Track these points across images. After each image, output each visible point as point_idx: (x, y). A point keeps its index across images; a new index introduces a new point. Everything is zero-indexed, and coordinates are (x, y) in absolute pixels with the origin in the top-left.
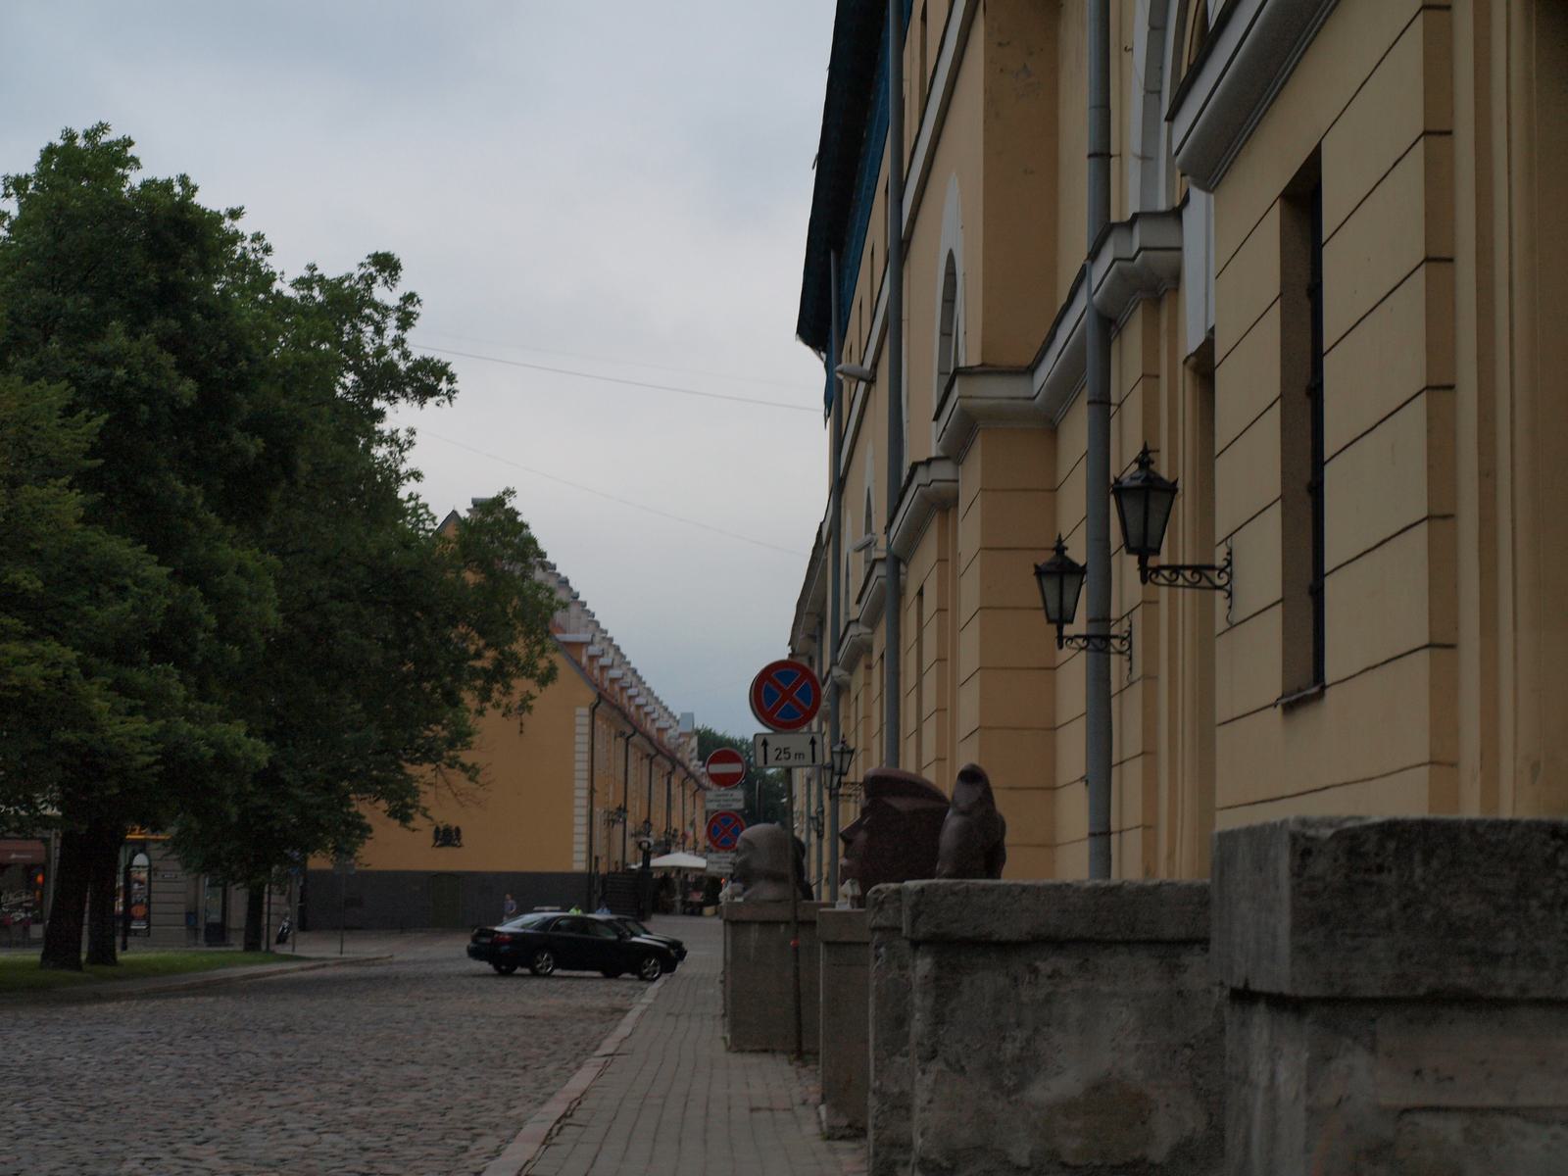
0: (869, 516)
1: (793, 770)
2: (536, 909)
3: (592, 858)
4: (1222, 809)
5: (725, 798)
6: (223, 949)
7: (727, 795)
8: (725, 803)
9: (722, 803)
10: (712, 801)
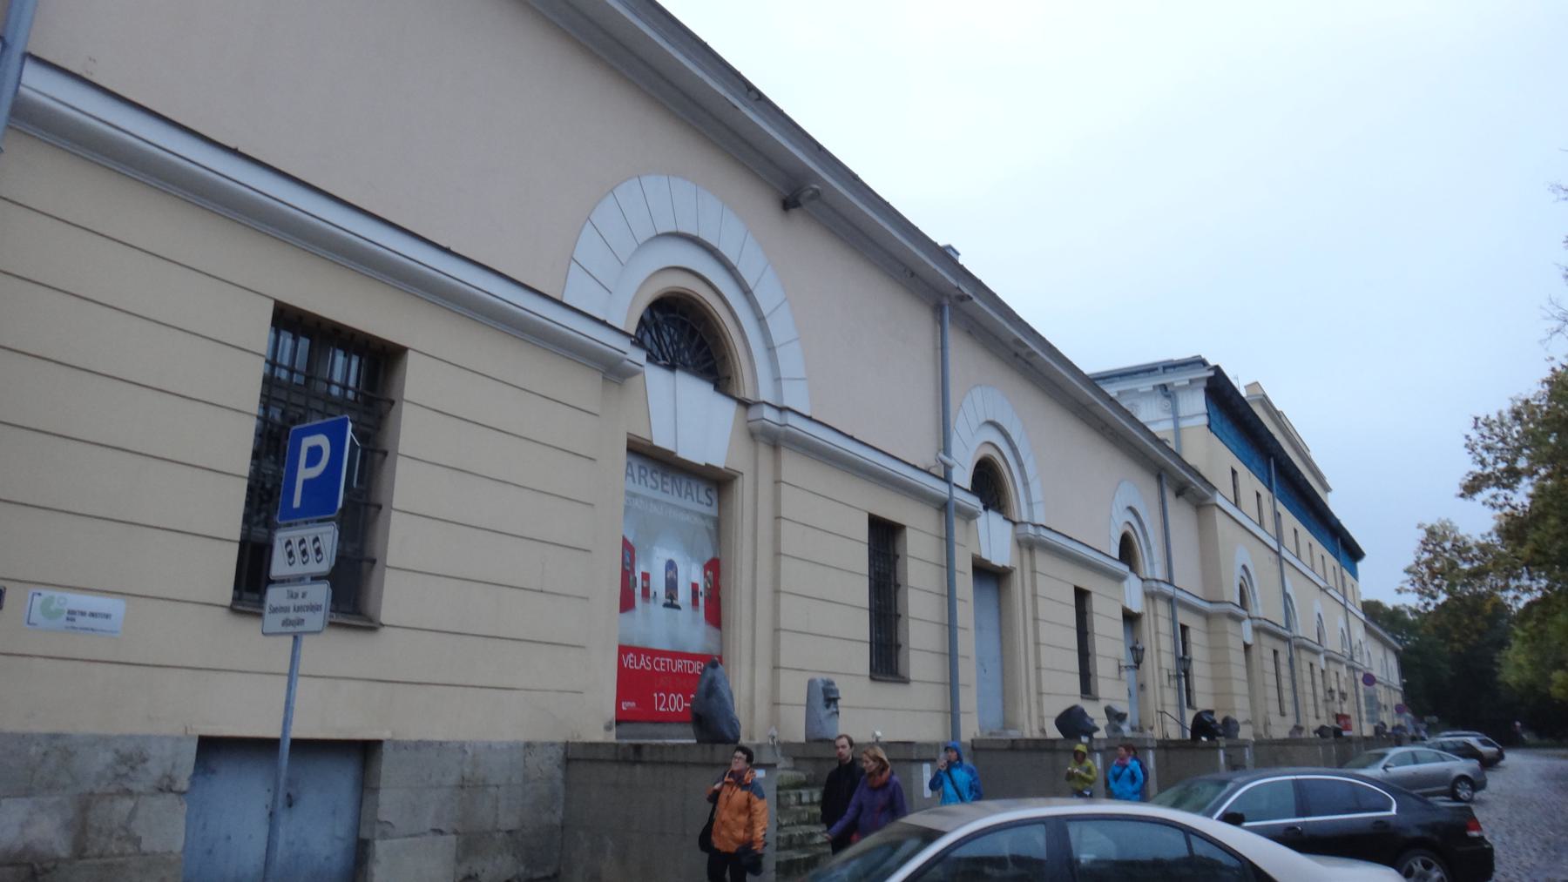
1: (361, 836)
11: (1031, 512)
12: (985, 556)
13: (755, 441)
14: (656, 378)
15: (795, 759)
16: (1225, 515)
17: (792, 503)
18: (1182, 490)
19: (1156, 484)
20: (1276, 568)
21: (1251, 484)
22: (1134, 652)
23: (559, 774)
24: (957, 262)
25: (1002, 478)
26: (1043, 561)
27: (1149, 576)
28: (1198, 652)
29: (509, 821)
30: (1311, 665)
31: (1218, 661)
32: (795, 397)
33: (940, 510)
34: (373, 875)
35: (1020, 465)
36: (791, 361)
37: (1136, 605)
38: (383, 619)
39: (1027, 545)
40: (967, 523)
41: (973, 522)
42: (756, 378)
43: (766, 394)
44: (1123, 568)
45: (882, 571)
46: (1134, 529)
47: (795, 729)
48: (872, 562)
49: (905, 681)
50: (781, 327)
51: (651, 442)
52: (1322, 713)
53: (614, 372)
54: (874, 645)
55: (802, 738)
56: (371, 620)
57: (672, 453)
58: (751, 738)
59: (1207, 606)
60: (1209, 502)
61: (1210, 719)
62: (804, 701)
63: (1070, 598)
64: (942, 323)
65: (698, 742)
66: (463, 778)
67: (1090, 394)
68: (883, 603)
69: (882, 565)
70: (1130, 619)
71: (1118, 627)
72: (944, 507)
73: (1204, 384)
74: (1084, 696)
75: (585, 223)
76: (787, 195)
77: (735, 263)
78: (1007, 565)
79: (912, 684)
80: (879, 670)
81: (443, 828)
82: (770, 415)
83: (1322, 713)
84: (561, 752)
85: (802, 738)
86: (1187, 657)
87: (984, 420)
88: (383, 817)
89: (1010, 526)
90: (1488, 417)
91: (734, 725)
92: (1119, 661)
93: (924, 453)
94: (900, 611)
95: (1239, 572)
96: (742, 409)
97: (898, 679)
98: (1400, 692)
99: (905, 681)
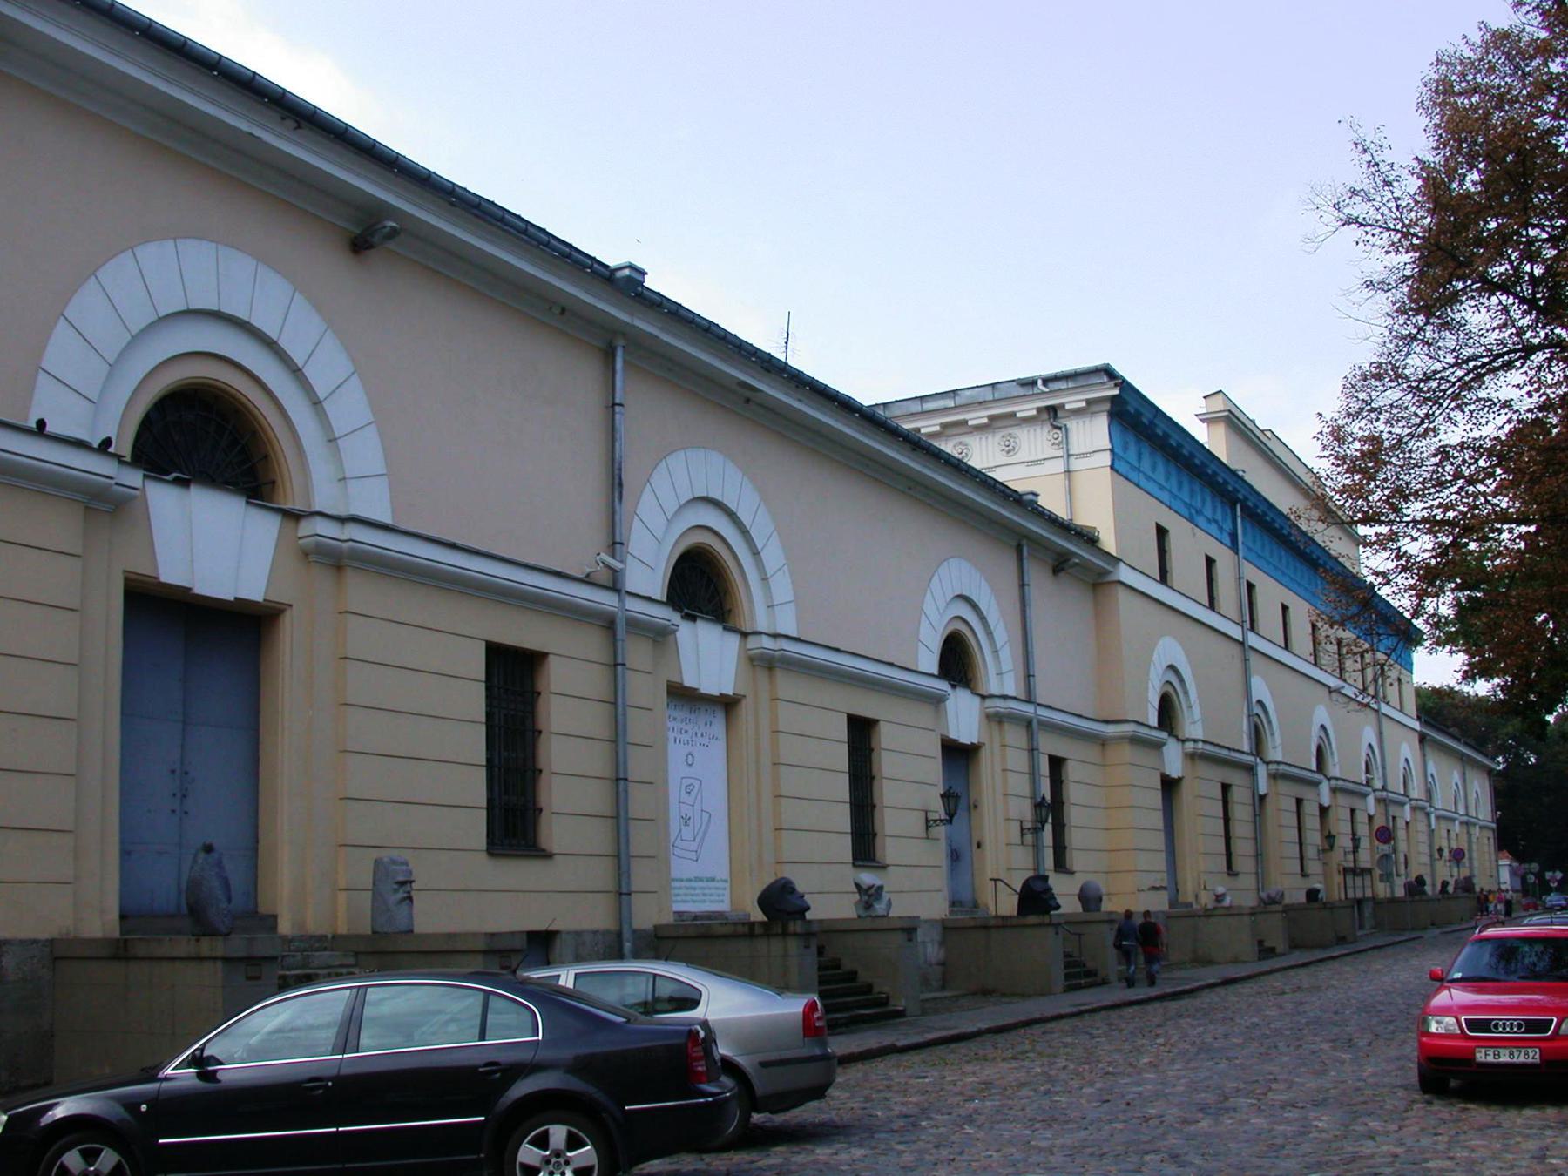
6: (1492, 848)
12: (953, 736)
18: (1060, 565)
19: (1015, 556)
20: (1237, 664)
25: (254, 416)
30: (1448, 831)
33: (609, 628)
35: (989, 633)
36: (782, 588)
44: (1164, 735)
51: (681, 684)
52: (1314, 867)
57: (695, 689)
58: (189, 940)
63: (841, 731)
67: (1101, 563)
70: (958, 755)
71: (932, 770)
73: (1107, 406)
75: (59, 318)
76: (358, 231)
78: (975, 741)
79: (1241, 876)
87: (952, 596)
89: (977, 700)
92: (1021, 822)
93: (584, 554)
95: (1402, 764)
98: (1493, 830)
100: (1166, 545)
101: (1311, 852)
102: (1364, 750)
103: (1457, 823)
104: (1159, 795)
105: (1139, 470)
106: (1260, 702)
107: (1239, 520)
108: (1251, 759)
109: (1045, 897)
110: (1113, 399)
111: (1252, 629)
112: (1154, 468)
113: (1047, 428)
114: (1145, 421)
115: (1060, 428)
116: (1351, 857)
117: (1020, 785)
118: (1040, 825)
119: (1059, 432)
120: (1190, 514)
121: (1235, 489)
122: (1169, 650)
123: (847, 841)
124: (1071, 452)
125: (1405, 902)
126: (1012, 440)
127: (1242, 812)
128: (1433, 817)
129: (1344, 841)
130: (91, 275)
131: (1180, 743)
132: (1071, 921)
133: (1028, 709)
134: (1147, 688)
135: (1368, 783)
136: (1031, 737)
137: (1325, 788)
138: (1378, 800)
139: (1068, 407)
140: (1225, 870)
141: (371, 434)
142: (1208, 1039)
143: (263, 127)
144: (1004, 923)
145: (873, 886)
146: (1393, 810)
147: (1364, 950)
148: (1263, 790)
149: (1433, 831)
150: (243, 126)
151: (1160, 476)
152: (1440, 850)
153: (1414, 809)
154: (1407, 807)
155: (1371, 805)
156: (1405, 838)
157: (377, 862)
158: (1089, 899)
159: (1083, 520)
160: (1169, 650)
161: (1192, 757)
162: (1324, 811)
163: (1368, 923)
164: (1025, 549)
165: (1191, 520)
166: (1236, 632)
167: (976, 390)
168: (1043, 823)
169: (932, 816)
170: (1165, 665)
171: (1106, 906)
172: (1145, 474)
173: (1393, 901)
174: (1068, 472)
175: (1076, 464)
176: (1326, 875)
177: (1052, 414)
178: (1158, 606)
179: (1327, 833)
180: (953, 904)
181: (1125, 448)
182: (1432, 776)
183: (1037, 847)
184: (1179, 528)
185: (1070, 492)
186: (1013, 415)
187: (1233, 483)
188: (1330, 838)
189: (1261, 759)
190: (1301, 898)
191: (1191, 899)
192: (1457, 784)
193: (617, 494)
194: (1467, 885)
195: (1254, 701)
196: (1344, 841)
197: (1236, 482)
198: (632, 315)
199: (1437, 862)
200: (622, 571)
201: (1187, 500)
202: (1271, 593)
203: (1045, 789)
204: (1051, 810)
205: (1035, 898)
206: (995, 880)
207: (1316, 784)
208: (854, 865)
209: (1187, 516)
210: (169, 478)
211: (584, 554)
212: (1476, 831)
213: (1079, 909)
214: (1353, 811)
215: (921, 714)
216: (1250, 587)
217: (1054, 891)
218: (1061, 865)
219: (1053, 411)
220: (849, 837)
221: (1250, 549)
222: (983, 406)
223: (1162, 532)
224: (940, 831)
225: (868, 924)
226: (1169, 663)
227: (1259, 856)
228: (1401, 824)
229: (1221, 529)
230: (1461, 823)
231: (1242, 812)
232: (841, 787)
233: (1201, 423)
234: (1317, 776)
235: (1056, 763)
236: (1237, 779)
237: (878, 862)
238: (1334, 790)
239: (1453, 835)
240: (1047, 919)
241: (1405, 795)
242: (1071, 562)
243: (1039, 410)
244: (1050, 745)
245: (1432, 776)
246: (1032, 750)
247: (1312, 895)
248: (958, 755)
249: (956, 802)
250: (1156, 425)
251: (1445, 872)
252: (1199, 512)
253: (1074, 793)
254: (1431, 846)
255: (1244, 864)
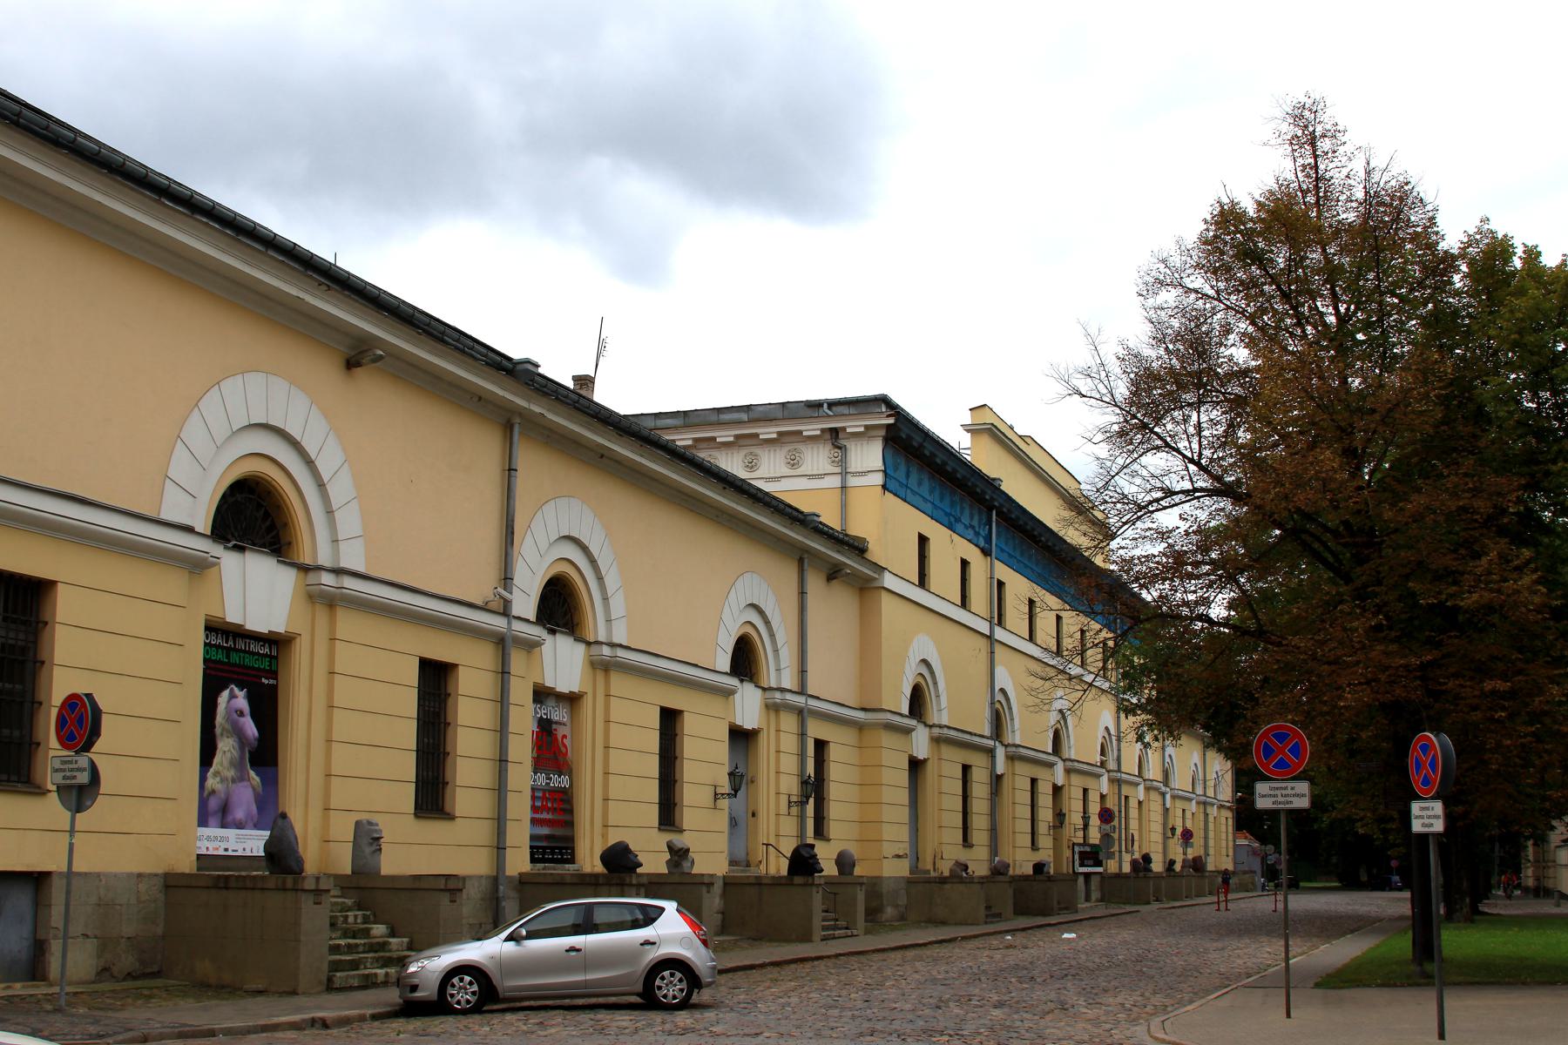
0: (818, 698)
1: (38, 937)
2: (1302, 884)
3: (631, 876)
4: (71, 846)
5: (1284, 792)
6: (1230, 829)
7: (1286, 788)
8: (1283, 799)
9: (1280, 799)
10: (1264, 796)
11: (609, 631)
12: (739, 722)
13: (313, 603)
14: (549, 640)
15: (342, 888)
16: (911, 603)
17: (346, 658)
20: (983, 656)
21: (949, 548)
22: (804, 786)
23: (161, 897)
24: (592, 401)
26: (619, 683)
27: (773, 685)
28: (837, 772)
29: (128, 930)
31: (869, 783)
32: (353, 558)
33: (498, 644)
34: (49, 963)
35: (772, 635)
36: (349, 521)
37: (921, 754)
38: (974, 843)
39: (602, 667)
40: (727, 699)
41: (732, 697)
42: (316, 544)
43: (324, 559)
44: (913, 722)
45: (432, 709)
46: (1003, 709)
47: (901, 869)
48: (422, 703)
49: (451, 817)
50: (340, 490)
52: (1045, 841)
53: (198, 567)
54: (420, 784)
55: (349, 872)
56: (39, 787)
59: (860, 715)
60: (877, 584)
61: (808, 853)
62: (352, 839)
64: (869, 588)
65: (271, 873)
66: (100, 898)
68: (431, 741)
69: (432, 704)
70: (741, 738)
71: (721, 750)
72: (501, 642)
73: (883, 433)
74: (662, 827)
77: (299, 439)
80: (425, 807)
81: (89, 933)
82: (327, 579)
83: (1045, 841)
84: (162, 880)
85: (349, 872)
86: (1087, 815)
88: (53, 924)
89: (759, 692)
90: (1537, 246)
91: (300, 862)
93: (481, 586)
94: (448, 749)
96: (302, 574)
97: (32, 790)
99: (451, 817)
100: (927, 551)
101: (1043, 828)
102: (1101, 732)
103: (1194, 802)
104: (906, 774)
105: (907, 486)
106: (1002, 690)
107: (994, 525)
108: (991, 743)
109: (811, 861)
110: (888, 426)
111: (1000, 623)
112: (920, 484)
113: (829, 446)
114: (915, 444)
115: (840, 448)
116: (1080, 834)
117: (789, 764)
118: (805, 799)
119: (839, 451)
120: (950, 522)
121: (992, 498)
122: (924, 645)
123: (655, 809)
124: (849, 470)
125: (1130, 877)
126: (797, 455)
127: (980, 790)
128: (1168, 797)
129: (1075, 818)
130: (194, 408)
131: (928, 729)
132: (830, 882)
133: (800, 700)
134: (902, 680)
135: (1103, 764)
136: (803, 724)
137: (1060, 768)
138: (1111, 781)
139: (848, 430)
140: (961, 842)
141: (355, 505)
142: (935, 973)
143: (306, 291)
144: (776, 882)
145: (682, 849)
146: (1125, 790)
147: (1081, 920)
148: (1000, 769)
149: (1167, 809)
150: (294, 291)
151: (925, 490)
152: (1173, 829)
153: (1147, 789)
154: (1141, 788)
155: (1104, 785)
156: (1137, 816)
157: (358, 824)
158: (845, 862)
159: (855, 530)
160: (924, 645)
161: (937, 741)
162: (1057, 790)
163: (1095, 895)
164: (806, 561)
165: (950, 527)
166: (984, 628)
167: (768, 406)
168: (808, 798)
169: (719, 790)
170: (918, 660)
171: (858, 871)
172: (912, 490)
173: (1119, 876)
174: (844, 488)
175: (853, 481)
176: (1057, 848)
177: (834, 434)
178: (913, 606)
179: (1058, 812)
180: (733, 863)
181: (896, 469)
182: (1170, 756)
183: (802, 818)
184: (939, 535)
185: (844, 506)
186: (800, 432)
187: (989, 492)
188: (1060, 816)
189: (1001, 742)
190: (1028, 870)
191: (929, 867)
192: (1196, 765)
193: (509, 540)
194: (1197, 865)
195: (997, 689)
196: (1075, 818)
197: (993, 492)
198: (529, 401)
199: (1171, 840)
200: (510, 602)
201: (948, 510)
202: (1019, 587)
203: (810, 770)
204: (814, 788)
205: (803, 862)
206: (767, 845)
207: (1051, 765)
208: (659, 829)
209: (947, 524)
210: (230, 545)
211: (481, 586)
212: (1213, 811)
213: (835, 873)
214: (1085, 791)
215: (713, 705)
216: (1001, 584)
217: (818, 857)
218: (820, 832)
219: (835, 433)
220: (657, 806)
221: (1002, 550)
222: (774, 422)
223: (923, 540)
224: (724, 803)
225: (676, 879)
226: (922, 658)
227: (994, 831)
228: (1133, 803)
229: (977, 534)
230: (1198, 803)
231: (980, 790)
232: (652, 766)
233: (965, 432)
234: (1053, 759)
235: (821, 745)
236: (978, 762)
237: (677, 827)
238: (1068, 771)
239: (1188, 815)
240: (810, 881)
241: (1140, 775)
242: (843, 572)
243: (823, 430)
244: (816, 730)
245: (1170, 756)
246: (802, 735)
247: (1039, 868)
248: (741, 738)
249: (739, 780)
250: (925, 447)
251: (1177, 853)
252: (958, 520)
253: (835, 772)
254: (1165, 824)
255: (980, 836)
